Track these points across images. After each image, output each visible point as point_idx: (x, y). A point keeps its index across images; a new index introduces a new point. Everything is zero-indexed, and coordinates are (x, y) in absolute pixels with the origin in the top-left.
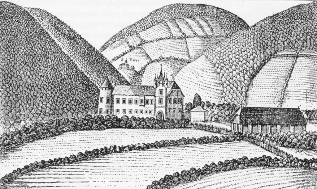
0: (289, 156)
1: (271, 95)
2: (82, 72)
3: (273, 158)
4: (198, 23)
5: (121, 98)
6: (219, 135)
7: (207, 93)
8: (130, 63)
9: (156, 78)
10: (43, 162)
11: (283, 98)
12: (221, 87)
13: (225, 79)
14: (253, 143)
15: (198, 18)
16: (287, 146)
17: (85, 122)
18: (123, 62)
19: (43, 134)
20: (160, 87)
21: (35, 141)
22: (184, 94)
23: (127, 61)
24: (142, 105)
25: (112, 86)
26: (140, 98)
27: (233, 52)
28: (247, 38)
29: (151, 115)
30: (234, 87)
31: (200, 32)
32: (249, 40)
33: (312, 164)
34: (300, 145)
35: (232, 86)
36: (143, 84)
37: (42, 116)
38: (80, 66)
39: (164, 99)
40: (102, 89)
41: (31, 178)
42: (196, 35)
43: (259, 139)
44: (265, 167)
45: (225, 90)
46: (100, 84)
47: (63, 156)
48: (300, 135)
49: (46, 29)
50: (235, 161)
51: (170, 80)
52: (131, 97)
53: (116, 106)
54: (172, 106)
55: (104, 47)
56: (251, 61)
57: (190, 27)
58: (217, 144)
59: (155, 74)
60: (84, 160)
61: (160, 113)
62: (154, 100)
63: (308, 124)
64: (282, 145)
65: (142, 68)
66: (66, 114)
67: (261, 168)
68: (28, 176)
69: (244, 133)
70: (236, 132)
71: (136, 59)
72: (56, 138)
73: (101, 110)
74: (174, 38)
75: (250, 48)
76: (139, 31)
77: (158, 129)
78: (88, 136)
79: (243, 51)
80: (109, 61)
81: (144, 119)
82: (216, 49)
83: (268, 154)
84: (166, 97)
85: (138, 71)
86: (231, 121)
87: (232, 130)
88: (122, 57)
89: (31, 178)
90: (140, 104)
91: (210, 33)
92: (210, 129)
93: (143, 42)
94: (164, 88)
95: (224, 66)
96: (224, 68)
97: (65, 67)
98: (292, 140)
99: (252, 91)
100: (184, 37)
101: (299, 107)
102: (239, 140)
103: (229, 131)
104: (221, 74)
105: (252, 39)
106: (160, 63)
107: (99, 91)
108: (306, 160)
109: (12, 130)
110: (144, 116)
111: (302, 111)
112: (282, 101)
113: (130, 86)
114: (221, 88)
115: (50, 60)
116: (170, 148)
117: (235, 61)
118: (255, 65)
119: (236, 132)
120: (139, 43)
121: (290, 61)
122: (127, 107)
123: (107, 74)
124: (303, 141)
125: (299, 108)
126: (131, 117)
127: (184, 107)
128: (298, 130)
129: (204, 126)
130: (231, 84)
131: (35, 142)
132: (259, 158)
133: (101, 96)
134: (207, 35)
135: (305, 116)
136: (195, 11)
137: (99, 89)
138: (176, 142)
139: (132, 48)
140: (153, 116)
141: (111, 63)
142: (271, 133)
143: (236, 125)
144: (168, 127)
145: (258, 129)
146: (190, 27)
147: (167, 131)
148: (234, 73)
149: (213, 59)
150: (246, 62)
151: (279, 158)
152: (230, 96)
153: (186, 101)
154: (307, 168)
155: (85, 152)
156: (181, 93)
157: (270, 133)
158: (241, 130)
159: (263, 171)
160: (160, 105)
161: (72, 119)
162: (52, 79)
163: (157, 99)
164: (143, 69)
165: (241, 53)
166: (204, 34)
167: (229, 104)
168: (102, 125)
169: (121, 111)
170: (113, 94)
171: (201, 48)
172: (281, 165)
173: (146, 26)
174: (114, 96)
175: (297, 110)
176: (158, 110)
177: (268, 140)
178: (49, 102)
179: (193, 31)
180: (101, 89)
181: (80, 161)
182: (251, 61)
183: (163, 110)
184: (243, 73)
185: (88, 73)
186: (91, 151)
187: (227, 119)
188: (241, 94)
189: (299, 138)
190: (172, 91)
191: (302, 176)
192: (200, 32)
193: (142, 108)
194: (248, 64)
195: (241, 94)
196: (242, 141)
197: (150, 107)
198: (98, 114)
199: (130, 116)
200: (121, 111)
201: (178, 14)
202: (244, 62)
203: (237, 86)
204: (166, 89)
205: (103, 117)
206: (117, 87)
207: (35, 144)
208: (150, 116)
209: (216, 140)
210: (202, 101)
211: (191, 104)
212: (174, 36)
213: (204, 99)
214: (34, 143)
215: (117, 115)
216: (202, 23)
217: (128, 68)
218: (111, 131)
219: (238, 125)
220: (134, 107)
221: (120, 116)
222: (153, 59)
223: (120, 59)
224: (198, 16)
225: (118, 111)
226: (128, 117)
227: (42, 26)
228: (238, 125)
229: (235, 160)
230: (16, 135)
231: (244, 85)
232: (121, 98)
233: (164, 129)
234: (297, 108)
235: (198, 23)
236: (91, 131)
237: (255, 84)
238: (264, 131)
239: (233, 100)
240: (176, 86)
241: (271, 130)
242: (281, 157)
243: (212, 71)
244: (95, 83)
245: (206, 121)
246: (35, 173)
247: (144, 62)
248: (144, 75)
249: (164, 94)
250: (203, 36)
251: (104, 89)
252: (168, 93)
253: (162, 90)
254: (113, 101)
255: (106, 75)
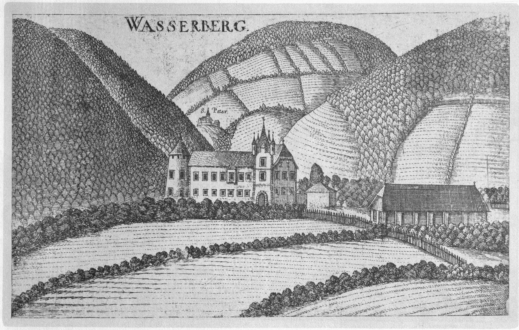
0: (461, 262)
1: (435, 166)
2: (138, 131)
3: (438, 265)
4: (302, 53)
5: (200, 171)
6: (353, 229)
7: (405, 164)
8: (215, 117)
9: (256, 139)
10: (81, 272)
11: (452, 170)
12: (357, 153)
13: (362, 141)
14: (405, 242)
15: (317, 44)
16: (457, 246)
17: (143, 209)
18: (204, 115)
19: (80, 227)
20: (262, 154)
21: (68, 239)
22: (298, 165)
23: (210, 112)
24: (232, 183)
25: (188, 152)
26: (229, 171)
27: (373, 97)
28: (393, 75)
29: (247, 198)
30: (374, 153)
31: (321, 67)
32: (397, 78)
33: (499, 273)
34: (477, 244)
35: (371, 151)
36: (233, 149)
37: (79, 200)
38: (135, 120)
39: (268, 174)
40: (173, 158)
41: (62, 298)
42: (314, 71)
43: (414, 234)
44: (424, 281)
45: (362, 157)
46: (170, 149)
47: (110, 264)
48: (477, 227)
49: (86, 63)
50: (375, 270)
51: (277, 142)
52: (215, 170)
53: (194, 185)
54: (281, 183)
55: (178, 89)
56: (400, 111)
57: (306, 59)
58: (351, 243)
59: (254, 133)
60: (140, 269)
61: (262, 194)
62: (252, 174)
63: (491, 210)
64: (452, 245)
65: (231, 124)
66: (116, 196)
67: (418, 281)
68: (55, 295)
69: (389, 226)
70: (377, 223)
71: (224, 109)
72: (101, 234)
73: (171, 190)
74: (283, 75)
75: (398, 90)
76: (227, 64)
77: (259, 219)
78: (148, 232)
79: (387, 96)
80: (185, 113)
81: (235, 205)
82: (349, 92)
83: (429, 258)
84: (272, 170)
85: (224, 128)
86: (371, 207)
87: (372, 220)
88: (203, 106)
89: (62, 298)
90: (228, 181)
91: (337, 67)
92: (342, 219)
93: (234, 82)
94: (268, 155)
95: (361, 119)
96: (361, 122)
97: (114, 122)
98: (466, 236)
99: (403, 158)
100: (297, 75)
101: (474, 183)
102: (382, 237)
103: (367, 223)
104: (356, 132)
105: (402, 76)
106: (263, 116)
107: (167, 160)
108: (487, 269)
109: (31, 221)
110: (237, 200)
111: (480, 190)
112: (450, 174)
113: (214, 152)
114: (357, 155)
115: (91, 111)
116: (278, 251)
117: (377, 112)
118: (407, 117)
119: (377, 223)
120: (227, 83)
121: (460, 111)
122: (210, 185)
123: (180, 134)
124: (481, 237)
125: (474, 186)
126: (215, 201)
127: (298, 184)
128: (475, 219)
129: (329, 214)
130: (370, 149)
131: (68, 241)
132: (415, 265)
133: (170, 167)
134: (333, 70)
135: (486, 197)
136: (312, 33)
137: (168, 156)
138: (286, 241)
139: (216, 92)
140: (250, 200)
141: (187, 116)
142: (434, 224)
143: (378, 212)
144: (275, 217)
145: (413, 219)
146: (306, 59)
147: (276, 223)
148: (375, 130)
149: (345, 109)
150: (391, 113)
151: (446, 264)
152: (369, 167)
153: (300, 176)
154: (490, 280)
155: (143, 257)
156: (294, 163)
157: (432, 225)
158: (384, 221)
159: (422, 285)
160: (262, 183)
161: (124, 204)
162: (95, 142)
163: (258, 173)
164: (234, 125)
165: (384, 99)
166: (328, 69)
167: (368, 179)
168: (173, 215)
169: (201, 192)
170: (189, 165)
171: (322, 92)
172: (449, 275)
173: (238, 58)
174: (191, 168)
175: (473, 188)
176: (258, 190)
177: (430, 236)
178: (89, 178)
179: (310, 65)
180: (171, 157)
181: (136, 271)
182: (400, 111)
183: (268, 190)
184: (387, 131)
185: (147, 132)
186: (154, 254)
187: (365, 203)
188: (385, 165)
189: (476, 232)
190: (281, 159)
191: (479, 293)
192: (321, 67)
193: (232, 187)
194: (394, 115)
195: (385, 165)
196: (387, 239)
197: (245, 185)
198: (166, 197)
199: (213, 199)
200: (201, 192)
201: (288, 37)
202: (389, 112)
203: (378, 151)
204: (272, 156)
205: (174, 201)
206: (194, 155)
207: (68, 243)
208: (245, 200)
209: (348, 237)
210: (324, 175)
211: (307, 179)
212: (283, 72)
213: (328, 172)
214: (66, 243)
215: (195, 199)
216: (308, 52)
217: (210, 124)
218: (187, 224)
219: (380, 212)
220: (220, 185)
221: (199, 199)
222: (251, 110)
223: (200, 110)
224: (317, 40)
225: (196, 192)
226: (210, 201)
227: (80, 57)
228: (380, 212)
229: (376, 268)
230: (36, 230)
231: (389, 149)
232: (200, 171)
233: (269, 220)
234: (472, 184)
235: (302, 53)
236: (154, 224)
237: (406, 147)
238: (423, 222)
239: (373, 172)
240: (285, 153)
241: (434, 220)
242: (449, 263)
243: (342, 128)
244: (160, 147)
245: (333, 207)
246: (68, 290)
247: (236, 114)
248: (235, 136)
249: (268, 165)
250: (326, 73)
251: (176, 157)
252: (274, 162)
253: (266, 157)
254: (190, 176)
255: (179, 135)
